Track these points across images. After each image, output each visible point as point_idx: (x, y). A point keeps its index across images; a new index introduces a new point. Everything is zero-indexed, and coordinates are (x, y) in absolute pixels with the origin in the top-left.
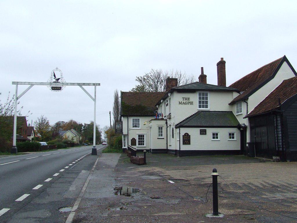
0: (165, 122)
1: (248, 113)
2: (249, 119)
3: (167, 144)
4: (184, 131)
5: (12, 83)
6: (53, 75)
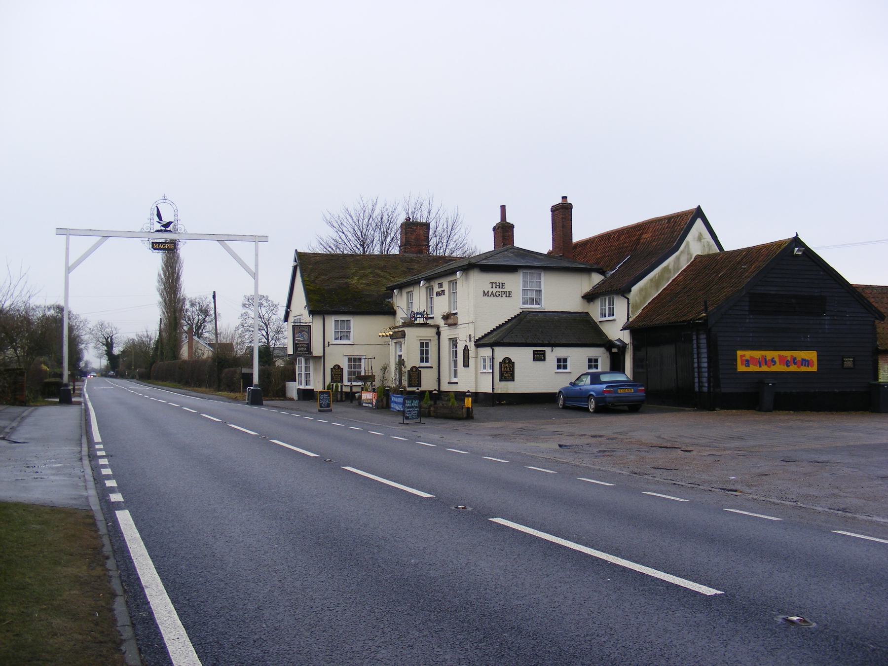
0: (434, 330)
1: (630, 320)
2: (631, 332)
3: (439, 379)
4: (502, 353)
5: (54, 231)
6: (156, 213)
